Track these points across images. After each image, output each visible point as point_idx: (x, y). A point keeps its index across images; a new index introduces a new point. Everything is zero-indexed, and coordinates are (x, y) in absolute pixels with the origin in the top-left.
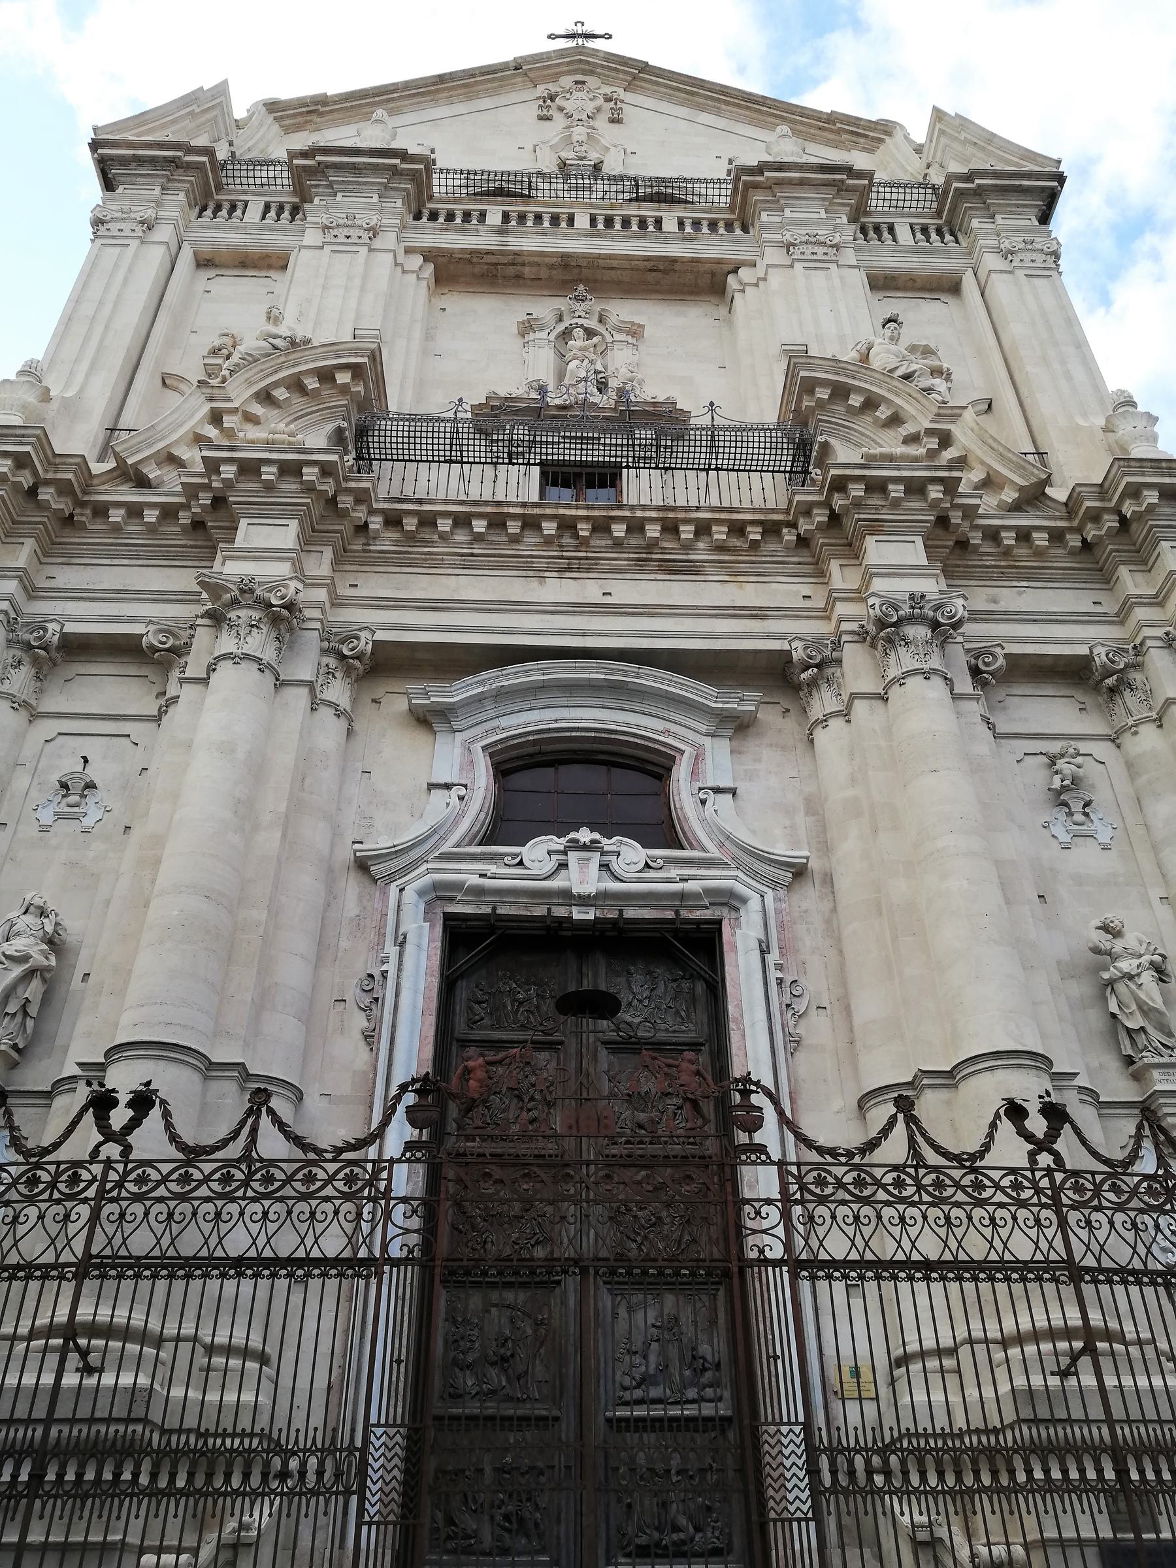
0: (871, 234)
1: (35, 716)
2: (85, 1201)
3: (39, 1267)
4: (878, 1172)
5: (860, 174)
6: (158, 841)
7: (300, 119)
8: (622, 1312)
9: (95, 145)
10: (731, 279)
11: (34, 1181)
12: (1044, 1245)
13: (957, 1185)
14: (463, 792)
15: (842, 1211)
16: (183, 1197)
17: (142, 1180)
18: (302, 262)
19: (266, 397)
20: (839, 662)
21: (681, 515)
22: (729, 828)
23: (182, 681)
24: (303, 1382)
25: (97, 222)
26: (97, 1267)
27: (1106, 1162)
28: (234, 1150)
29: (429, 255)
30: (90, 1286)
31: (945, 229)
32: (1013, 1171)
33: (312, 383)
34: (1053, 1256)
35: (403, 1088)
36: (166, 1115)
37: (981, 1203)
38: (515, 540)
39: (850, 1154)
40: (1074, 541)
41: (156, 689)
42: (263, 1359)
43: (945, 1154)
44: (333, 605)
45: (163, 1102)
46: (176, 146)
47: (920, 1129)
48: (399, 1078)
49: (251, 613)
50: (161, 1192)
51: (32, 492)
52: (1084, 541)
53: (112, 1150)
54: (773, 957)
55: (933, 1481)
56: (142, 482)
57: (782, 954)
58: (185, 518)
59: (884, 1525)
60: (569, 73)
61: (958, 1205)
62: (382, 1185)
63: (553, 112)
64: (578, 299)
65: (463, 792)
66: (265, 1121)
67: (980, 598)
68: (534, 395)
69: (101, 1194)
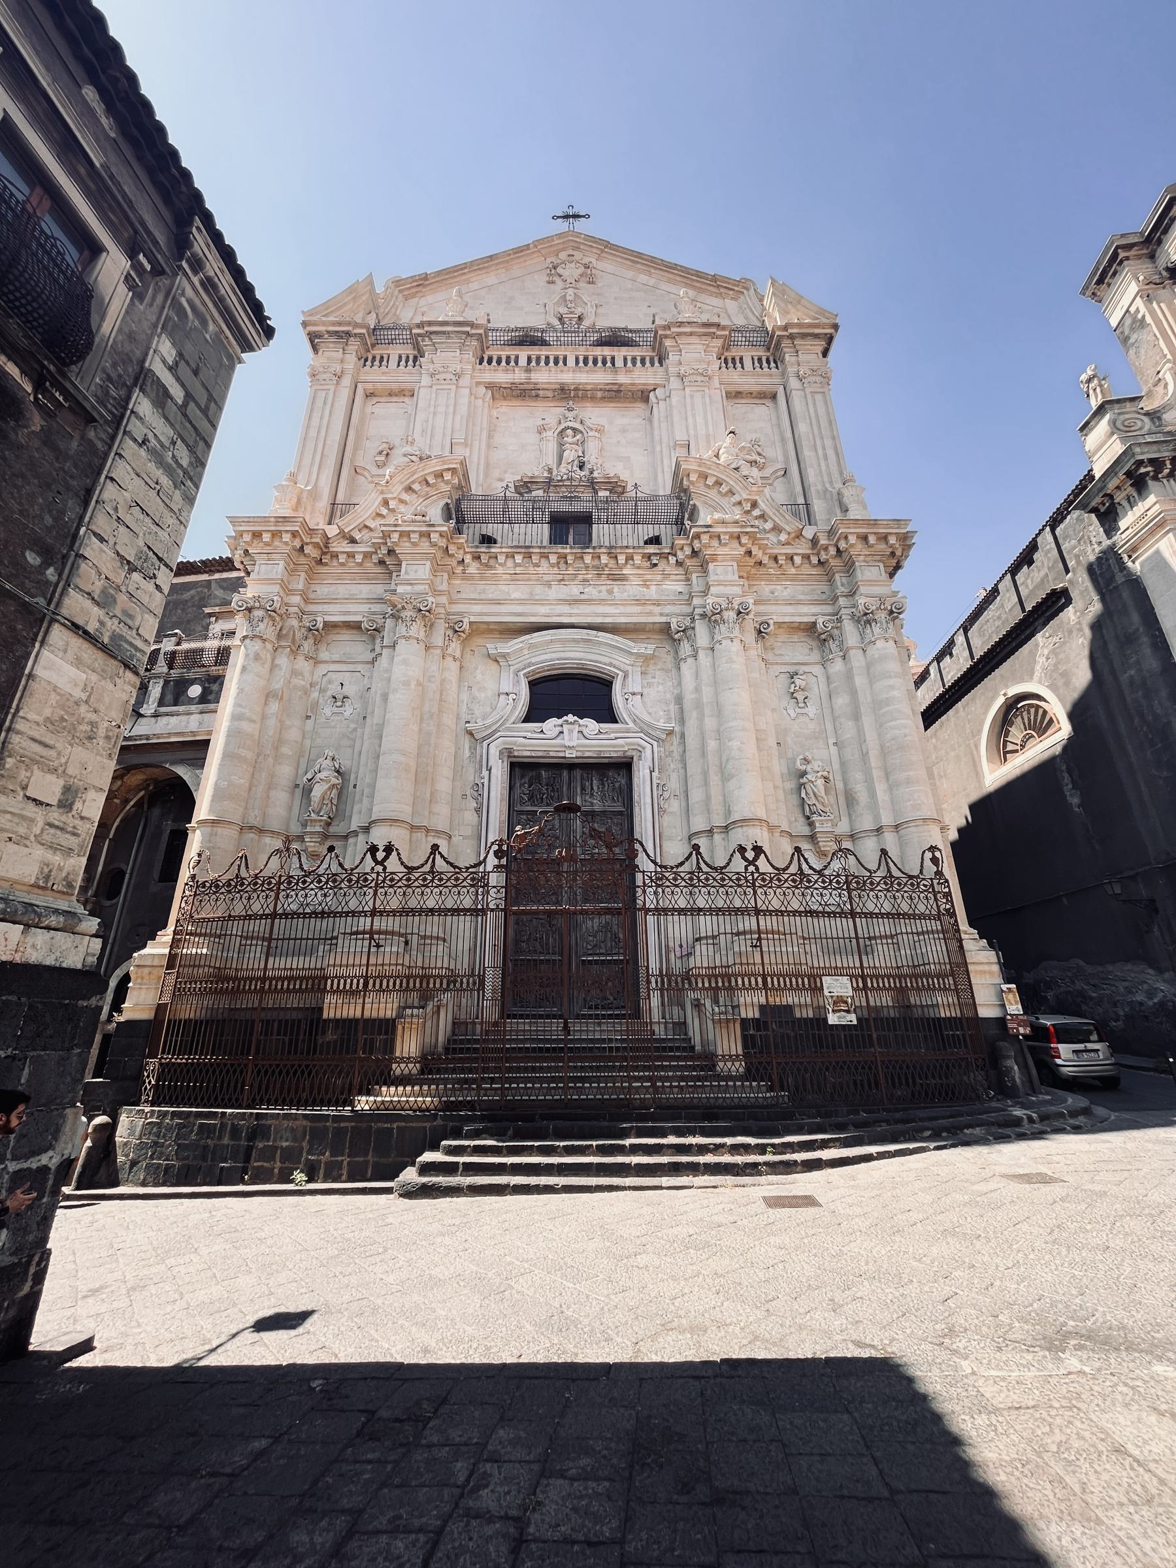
4: (682, 875)
6: (381, 727)
7: (414, 290)
9: (305, 324)
10: (652, 395)
11: (350, 881)
13: (714, 879)
16: (408, 886)
18: (423, 394)
19: (409, 489)
20: (693, 628)
22: (638, 713)
28: (427, 868)
31: (771, 359)
32: (738, 873)
33: (431, 480)
35: (492, 844)
36: (399, 854)
37: (723, 886)
39: (672, 868)
40: (814, 560)
41: (370, 647)
43: (710, 867)
46: (349, 324)
48: (491, 839)
50: (400, 884)
51: (302, 548)
53: (379, 868)
54: (655, 774)
56: (353, 541)
58: (375, 559)
63: (556, 279)
66: (438, 857)
68: (546, 474)
69: (377, 885)
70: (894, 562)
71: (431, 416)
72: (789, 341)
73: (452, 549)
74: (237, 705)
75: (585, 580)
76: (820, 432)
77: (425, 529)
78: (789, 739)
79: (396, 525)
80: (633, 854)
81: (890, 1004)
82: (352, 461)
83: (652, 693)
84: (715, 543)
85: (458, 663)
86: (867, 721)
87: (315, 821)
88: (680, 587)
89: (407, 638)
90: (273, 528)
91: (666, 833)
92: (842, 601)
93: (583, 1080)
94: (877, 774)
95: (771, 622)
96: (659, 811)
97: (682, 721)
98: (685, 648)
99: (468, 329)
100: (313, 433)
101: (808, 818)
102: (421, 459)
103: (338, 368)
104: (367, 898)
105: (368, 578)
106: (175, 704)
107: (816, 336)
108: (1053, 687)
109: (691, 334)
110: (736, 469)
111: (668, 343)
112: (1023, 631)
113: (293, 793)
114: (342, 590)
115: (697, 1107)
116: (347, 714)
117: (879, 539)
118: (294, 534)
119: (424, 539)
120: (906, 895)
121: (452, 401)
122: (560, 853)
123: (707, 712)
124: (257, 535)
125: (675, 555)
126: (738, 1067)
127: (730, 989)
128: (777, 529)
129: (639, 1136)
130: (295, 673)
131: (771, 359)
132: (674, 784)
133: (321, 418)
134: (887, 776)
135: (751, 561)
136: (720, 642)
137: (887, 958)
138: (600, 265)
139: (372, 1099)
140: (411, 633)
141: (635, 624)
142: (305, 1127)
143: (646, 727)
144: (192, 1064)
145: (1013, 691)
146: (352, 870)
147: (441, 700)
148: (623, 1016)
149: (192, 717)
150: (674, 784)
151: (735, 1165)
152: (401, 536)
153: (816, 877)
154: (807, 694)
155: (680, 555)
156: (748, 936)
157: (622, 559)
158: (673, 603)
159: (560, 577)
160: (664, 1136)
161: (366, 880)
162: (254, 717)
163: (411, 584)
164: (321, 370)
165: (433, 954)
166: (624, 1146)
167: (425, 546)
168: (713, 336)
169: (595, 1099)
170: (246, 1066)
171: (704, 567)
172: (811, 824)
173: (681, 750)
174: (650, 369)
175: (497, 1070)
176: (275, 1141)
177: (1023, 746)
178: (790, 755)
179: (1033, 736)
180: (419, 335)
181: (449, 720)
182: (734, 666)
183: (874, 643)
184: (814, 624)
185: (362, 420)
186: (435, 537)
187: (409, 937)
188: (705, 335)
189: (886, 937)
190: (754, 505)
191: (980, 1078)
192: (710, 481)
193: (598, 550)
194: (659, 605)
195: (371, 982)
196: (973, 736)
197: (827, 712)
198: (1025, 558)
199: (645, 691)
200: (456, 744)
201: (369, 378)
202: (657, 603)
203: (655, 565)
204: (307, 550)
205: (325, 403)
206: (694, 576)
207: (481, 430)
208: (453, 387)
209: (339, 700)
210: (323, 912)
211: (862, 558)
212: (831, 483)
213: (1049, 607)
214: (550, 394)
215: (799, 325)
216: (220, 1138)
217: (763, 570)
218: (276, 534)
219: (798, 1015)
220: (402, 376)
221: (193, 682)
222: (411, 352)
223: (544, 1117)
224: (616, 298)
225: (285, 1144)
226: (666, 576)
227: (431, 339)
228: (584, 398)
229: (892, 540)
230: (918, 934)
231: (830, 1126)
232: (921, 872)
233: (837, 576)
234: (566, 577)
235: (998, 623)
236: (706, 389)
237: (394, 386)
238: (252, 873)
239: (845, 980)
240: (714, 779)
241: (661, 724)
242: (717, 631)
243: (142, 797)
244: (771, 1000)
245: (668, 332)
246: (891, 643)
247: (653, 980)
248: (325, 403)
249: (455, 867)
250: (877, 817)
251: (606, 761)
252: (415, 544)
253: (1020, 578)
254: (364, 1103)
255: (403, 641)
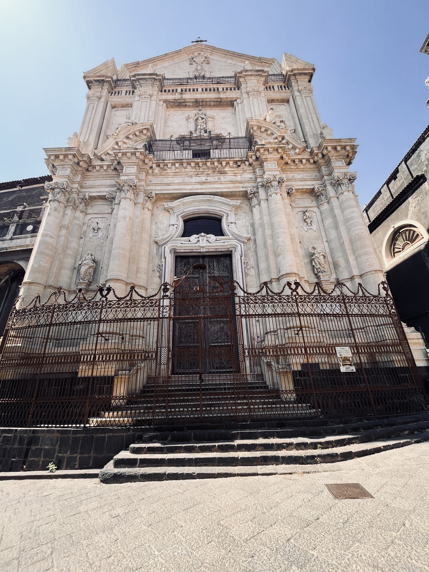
0: (268, 89)
1: (86, 214)
2: (99, 309)
3: (91, 321)
5: (265, 72)
6: (112, 239)
7: (133, 69)
8: (213, 327)
9: (85, 77)
10: (235, 102)
11: (89, 306)
12: (293, 310)
13: (276, 299)
14: (177, 226)
15: (252, 305)
16: (118, 307)
17: (110, 304)
18: (135, 104)
19: (127, 138)
20: (258, 192)
21: (222, 160)
22: (233, 231)
23: (115, 204)
24: (151, 341)
25: (88, 98)
26: (102, 321)
27: (308, 293)
28: (128, 298)
29: (165, 101)
30: (101, 324)
31: (286, 86)
32: (288, 296)
33: (138, 133)
34: (295, 312)
36: (114, 292)
37: (280, 302)
38: (186, 168)
39: (254, 294)
40: (312, 161)
41: (111, 207)
42: (143, 337)
44: (146, 186)
45: (113, 289)
46: (103, 76)
47: (269, 288)
49: (127, 188)
50: (114, 306)
51: (78, 163)
52: (314, 161)
53: (104, 299)
54: (243, 258)
55: (271, 353)
56: (102, 160)
57: (245, 257)
58: (112, 167)
59: (262, 362)
60: (196, 51)
61: (276, 303)
62: (158, 304)
64: (200, 110)
65: (177, 226)
66: (134, 292)
67: (290, 175)
69: (102, 307)
70: (348, 160)
71: (139, 112)
72: (294, 77)
73: (147, 161)
74: (45, 230)
75: (208, 174)
76: (310, 112)
77: (133, 151)
78: (305, 241)
79: (120, 150)
80: (234, 288)
81: (366, 361)
82: (105, 133)
83: (240, 223)
84: (266, 153)
85: (150, 212)
86: (342, 229)
87: (82, 283)
88: (251, 176)
89: (125, 198)
90: (64, 153)
91: (249, 284)
92: (326, 178)
93: (210, 406)
94: (349, 252)
95: (294, 188)
96: (245, 274)
97: (254, 234)
98: (255, 201)
99: (155, 77)
100: (87, 120)
101: (316, 275)
102: (133, 124)
103: (99, 95)
104: (97, 314)
105: (110, 177)
106: (21, 234)
107: (305, 74)
108: (418, 220)
109: (251, 75)
110: (274, 123)
111: (241, 80)
112: (401, 198)
113: (73, 272)
114: (98, 183)
115: (274, 420)
116: (99, 236)
117: (342, 148)
118: (74, 156)
119: (133, 156)
120: (373, 305)
121: (148, 106)
122: (196, 289)
123: (266, 227)
124: (57, 157)
125: (248, 161)
126: (293, 397)
127: (285, 356)
128: (294, 148)
129: (242, 438)
130: (75, 218)
131: (286, 86)
132: (252, 262)
133: (91, 114)
134: (354, 253)
135: (283, 162)
136: (271, 195)
137: (362, 338)
138: (211, 57)
139: (99, 419)
140: (127, 196)
141: (231, 192)
142: (58, 437)
143: (237, 237)
144: (4, 403)
145: (397, 225)
146: (90, 300)
147: (142, 227)
148: (231, 372)
149: (28, 239)
150: (252, 262)
151: (301, 457)
152: (123, 155)
153: (328, 297)
154: (312, 220)
155: (251, 160)
156: (295, 329)
157: (224, 163)
158: (248, 182)
159: (196, 173)
160: (256, 438)
161: (97, 305)
162: (53, 236)
163: (127, 176)
164: (92, 95)
165: (137, 344)
166: (234, 445)
167: (134, 159)
168: (261, 76)
169: (217, 417)
170: (31, 403)
171: (261, 166)
172: (318, 277)
173: (254, 247)
174: (234, 91)
175: (163, 401)
176: (41, 445)
177: (403, 249)
178: (306, 247)
179: (409, 244)
180: (134, 80)
181: (146, 236)
182: (278, 205)
183: (343, 193)
184: (313, 189)
185: (110, 116)
186: (138, 154)
187: (124, 336)
188: (257, 75)
189: (361, 329)
190: (283, 138)
191: (422, 399)
192: (263, 130)
193: (213, 160)
194: (242, 183)
195: (97, 356)
196: (378, 248)
197: (322, 228)
198: (393, 177)
199: (237, 222)
200: (150, 247)
201: (113, 100)
202: (241, 182)
203: (239, 166)
204: (81, 163)
205: (93, 109)
206: (257, 169)
207: (161, 118)
208: (149, 100)
209: (96, 230)
210: (75, 322)
211: (334, 157)
212: (316, 131)
213: (415, 185)
214: (191, 104)
215: (298, 69)
216: (13, 444)
217: (288, 167)
218: (66, 156)
219: (321, 368)
220: (127, 99)
221: (29, 224)
222: (131, 89)
223: (189, 428)
224: (219, 69)
225: (46, 447)
226: (244, 171)
227: (139, 82)
228: (206, 106)
229: (348, 148)
230: (377, 326)
231: (350, 429)
232: (379, 294)
233: (323, 167)
234: (199, 173)
235: (381, 206)
236: (259, 97)
237: (124, 103)
238: (41, 304)
239: (347, 348)
240: (271, 257)
241: (245, 235)
242: (269, 191)
243: (8, 279)
244: (310, 361)
245: (241, 75)
246: (351, 193)
247: (246, 351)
248: (93, 109)
249: (142, 297)
250: (351, 272)
251: (219, 253)
252: (129, 158)
253: (391, 185)
254: (94, 422)
255: (123, 200)
